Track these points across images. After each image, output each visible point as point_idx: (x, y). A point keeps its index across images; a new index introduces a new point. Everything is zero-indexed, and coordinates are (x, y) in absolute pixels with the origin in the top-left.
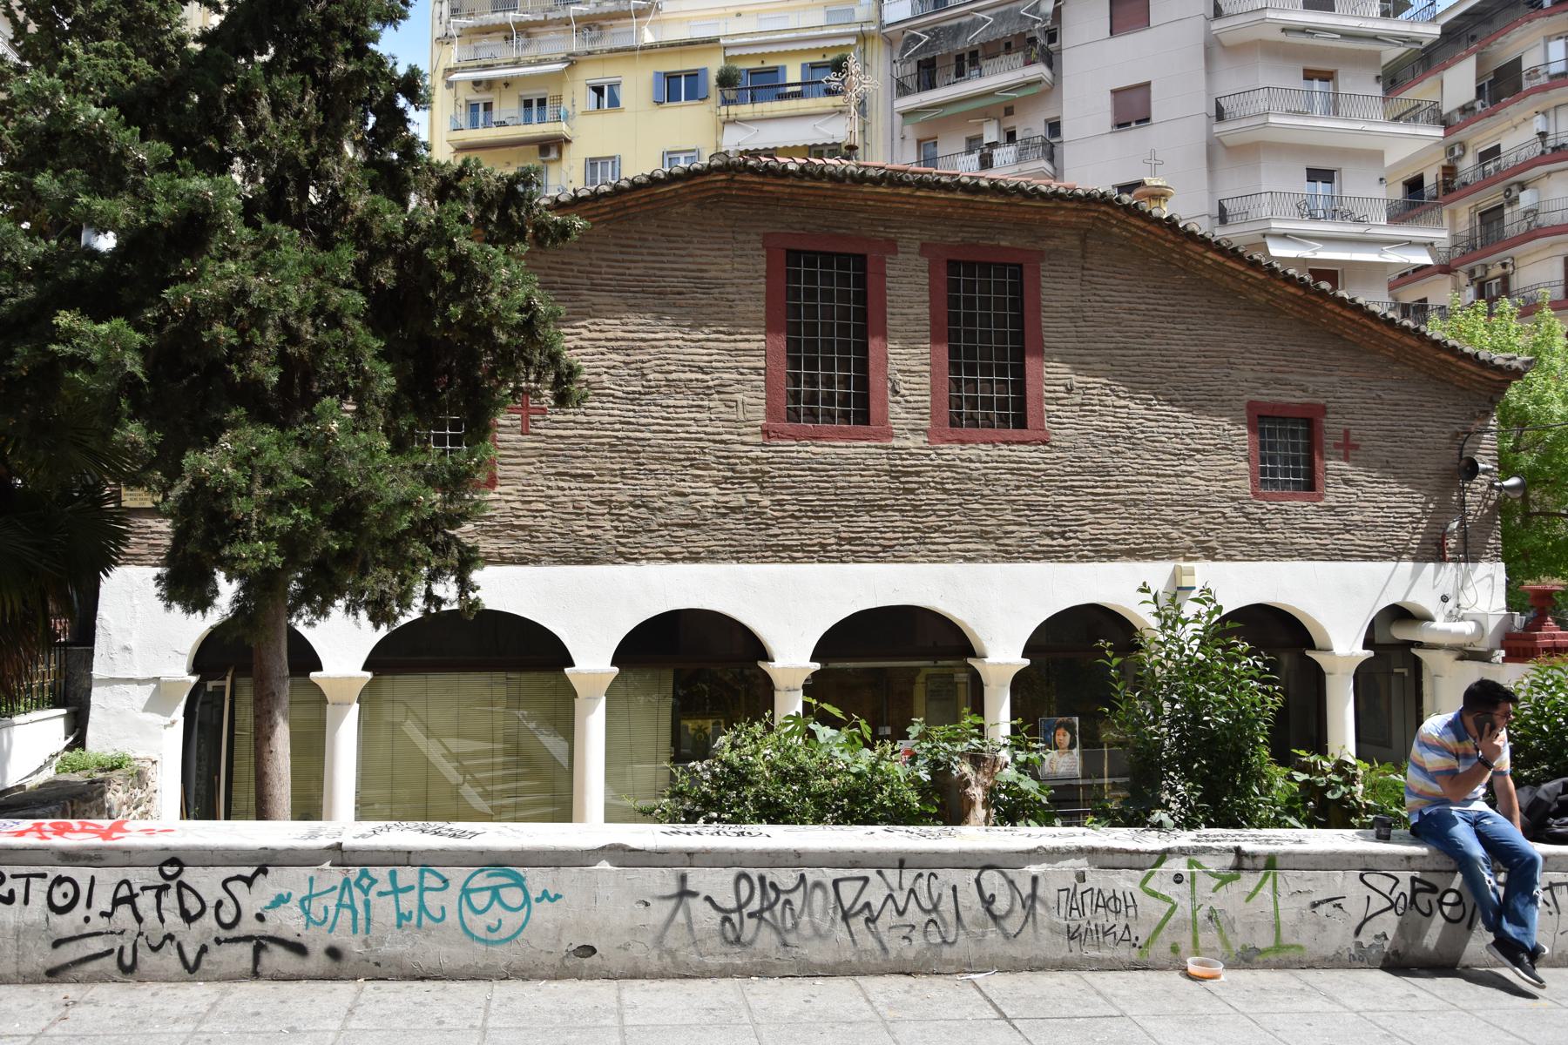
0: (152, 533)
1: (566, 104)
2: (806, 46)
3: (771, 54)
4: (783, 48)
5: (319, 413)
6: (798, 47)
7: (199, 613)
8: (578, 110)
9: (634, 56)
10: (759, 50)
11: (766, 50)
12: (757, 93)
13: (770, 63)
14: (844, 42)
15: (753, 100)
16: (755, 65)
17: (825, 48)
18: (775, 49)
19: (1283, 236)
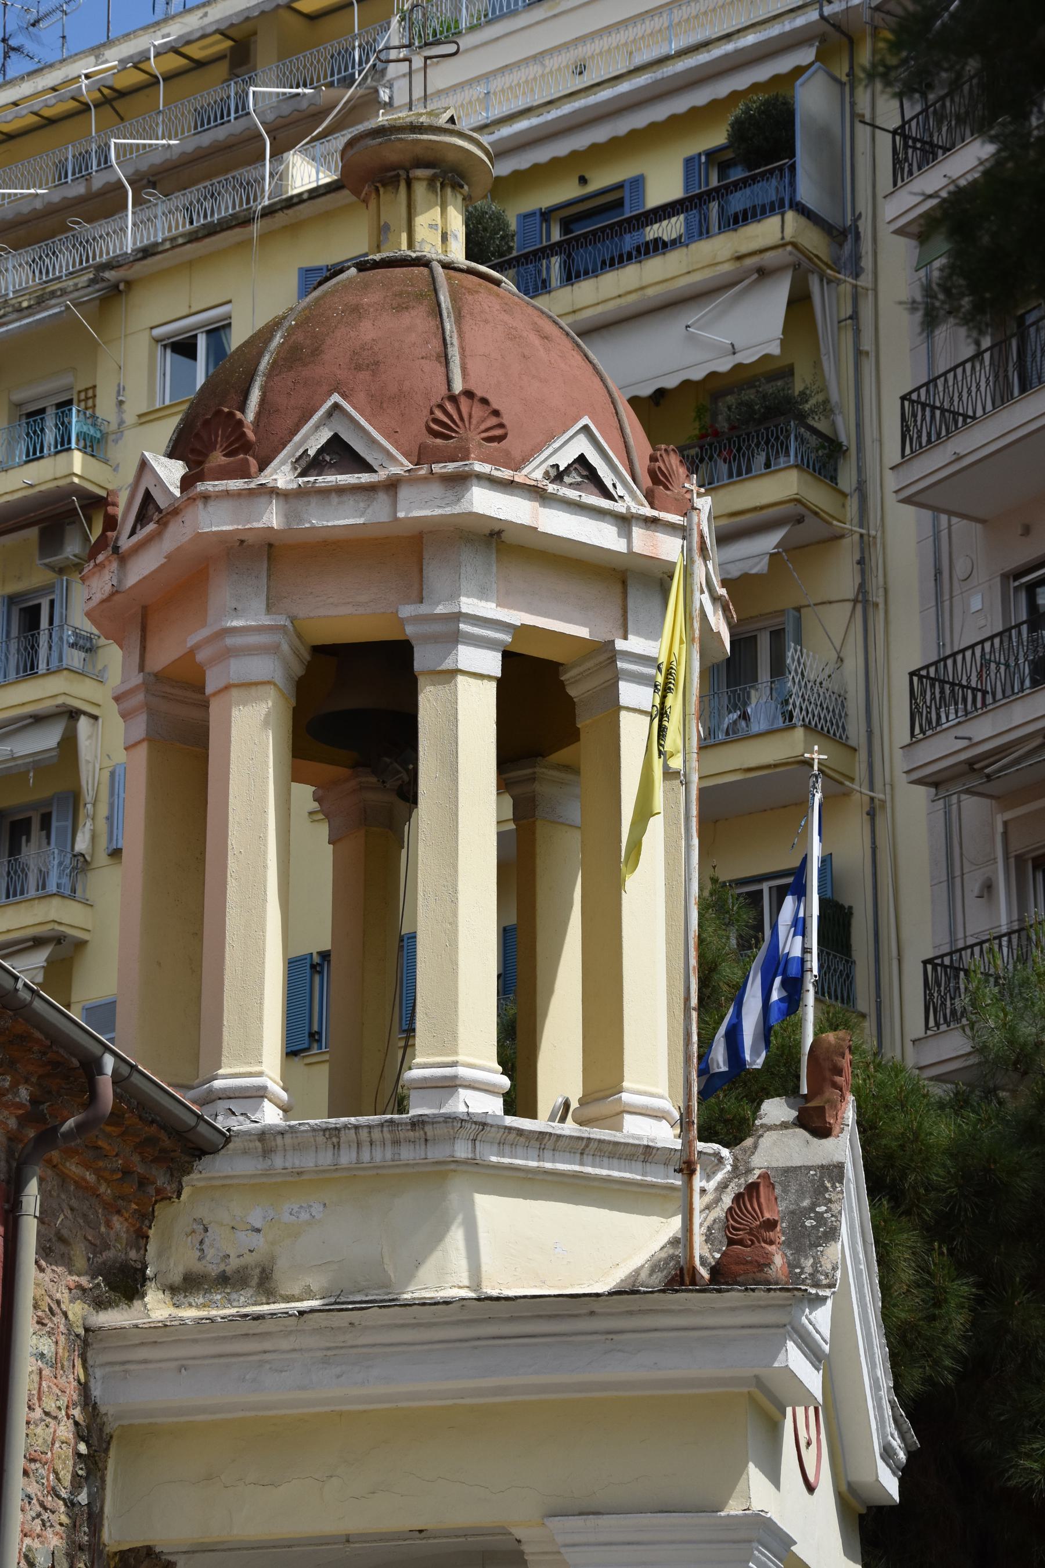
0: (749, 459)
1: (105, 408)
2: (680, 105)
3: (595, 149)
4: (622, 126)
5: (802, 393)
6: (660, 113)
7: (315, 806)
8: (130, 418)
9: (245, 244)
10: (561, 148)
11: (581, 141)
12: (583, 257)
13: (602, 179)
14: (783, 65)
15: (570, 277)
16: (565, 191)
17: (575, 155)
18: (600, 134)
19: (533, 1554)
